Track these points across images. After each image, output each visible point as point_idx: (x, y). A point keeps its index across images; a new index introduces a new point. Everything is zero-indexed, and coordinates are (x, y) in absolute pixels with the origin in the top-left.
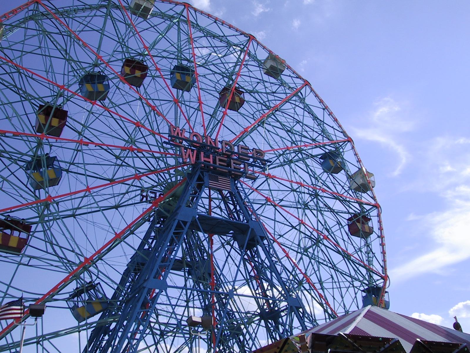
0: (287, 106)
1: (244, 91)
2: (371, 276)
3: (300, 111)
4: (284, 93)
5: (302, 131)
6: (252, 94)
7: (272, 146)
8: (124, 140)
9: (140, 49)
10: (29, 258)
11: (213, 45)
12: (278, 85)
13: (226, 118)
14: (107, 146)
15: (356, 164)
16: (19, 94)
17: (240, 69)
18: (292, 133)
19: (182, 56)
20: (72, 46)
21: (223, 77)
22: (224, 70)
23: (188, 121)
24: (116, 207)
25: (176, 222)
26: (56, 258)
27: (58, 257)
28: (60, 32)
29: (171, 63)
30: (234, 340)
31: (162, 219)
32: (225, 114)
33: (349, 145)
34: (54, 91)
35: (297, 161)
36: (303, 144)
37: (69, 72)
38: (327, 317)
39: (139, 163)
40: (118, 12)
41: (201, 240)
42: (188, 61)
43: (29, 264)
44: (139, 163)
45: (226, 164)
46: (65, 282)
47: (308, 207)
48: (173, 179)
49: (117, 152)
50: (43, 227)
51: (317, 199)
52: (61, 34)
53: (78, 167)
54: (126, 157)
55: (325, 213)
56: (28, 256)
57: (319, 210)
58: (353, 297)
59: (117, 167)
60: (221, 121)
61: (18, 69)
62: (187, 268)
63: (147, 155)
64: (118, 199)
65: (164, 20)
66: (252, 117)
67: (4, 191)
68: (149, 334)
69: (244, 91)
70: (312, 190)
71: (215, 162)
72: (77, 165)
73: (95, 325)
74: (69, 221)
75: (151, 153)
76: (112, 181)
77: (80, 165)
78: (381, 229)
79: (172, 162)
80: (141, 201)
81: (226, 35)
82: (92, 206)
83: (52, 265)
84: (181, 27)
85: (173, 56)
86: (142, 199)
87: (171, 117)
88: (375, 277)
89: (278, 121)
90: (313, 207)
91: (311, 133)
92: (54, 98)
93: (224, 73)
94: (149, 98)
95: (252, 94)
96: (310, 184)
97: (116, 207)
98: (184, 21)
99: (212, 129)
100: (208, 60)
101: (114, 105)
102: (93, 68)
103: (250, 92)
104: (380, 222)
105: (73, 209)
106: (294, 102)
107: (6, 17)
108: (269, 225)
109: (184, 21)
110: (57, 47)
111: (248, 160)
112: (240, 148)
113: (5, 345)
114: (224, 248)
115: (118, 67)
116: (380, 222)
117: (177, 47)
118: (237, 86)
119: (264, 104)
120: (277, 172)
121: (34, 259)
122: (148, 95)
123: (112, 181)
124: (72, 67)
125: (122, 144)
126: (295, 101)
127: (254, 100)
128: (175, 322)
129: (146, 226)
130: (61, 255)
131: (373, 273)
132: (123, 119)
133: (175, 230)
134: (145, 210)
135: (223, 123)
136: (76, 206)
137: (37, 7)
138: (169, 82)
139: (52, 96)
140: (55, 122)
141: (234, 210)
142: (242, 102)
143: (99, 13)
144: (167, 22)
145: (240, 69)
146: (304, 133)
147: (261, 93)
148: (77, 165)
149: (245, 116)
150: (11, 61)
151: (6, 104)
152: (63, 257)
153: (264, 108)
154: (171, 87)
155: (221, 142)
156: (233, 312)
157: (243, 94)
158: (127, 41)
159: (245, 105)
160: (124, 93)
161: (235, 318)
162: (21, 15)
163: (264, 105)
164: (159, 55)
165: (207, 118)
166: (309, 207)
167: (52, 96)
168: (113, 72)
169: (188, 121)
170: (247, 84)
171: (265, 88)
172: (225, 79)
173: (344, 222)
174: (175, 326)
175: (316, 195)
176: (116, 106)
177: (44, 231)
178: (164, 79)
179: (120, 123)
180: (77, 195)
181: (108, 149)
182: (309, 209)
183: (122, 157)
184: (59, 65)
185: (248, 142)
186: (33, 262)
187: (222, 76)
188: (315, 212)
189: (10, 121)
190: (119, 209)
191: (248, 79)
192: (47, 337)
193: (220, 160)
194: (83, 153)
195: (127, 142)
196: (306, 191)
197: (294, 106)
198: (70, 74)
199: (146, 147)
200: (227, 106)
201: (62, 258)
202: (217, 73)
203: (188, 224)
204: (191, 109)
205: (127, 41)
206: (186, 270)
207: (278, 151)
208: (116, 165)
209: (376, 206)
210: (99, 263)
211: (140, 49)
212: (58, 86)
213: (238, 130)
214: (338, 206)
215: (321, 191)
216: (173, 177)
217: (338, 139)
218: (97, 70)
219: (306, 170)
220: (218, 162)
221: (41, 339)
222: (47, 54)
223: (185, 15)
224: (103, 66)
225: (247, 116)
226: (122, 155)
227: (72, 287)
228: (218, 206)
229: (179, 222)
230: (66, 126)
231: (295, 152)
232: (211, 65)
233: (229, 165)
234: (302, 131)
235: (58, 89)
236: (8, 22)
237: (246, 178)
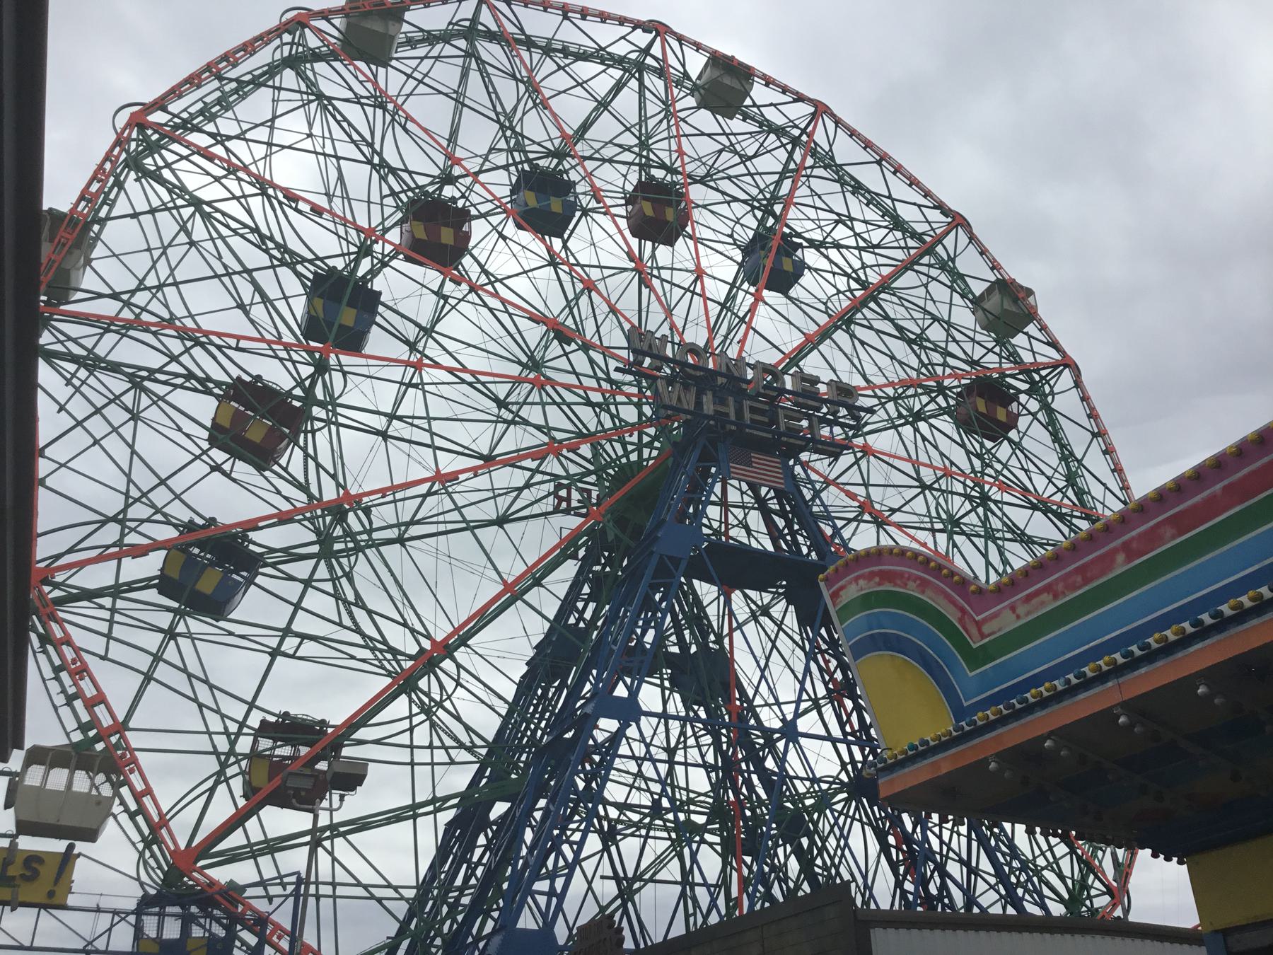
0: (909, 279)
1: (805, 244)
3: (940, 292)
4: (900, 248)
5: (947, 342)
6: (822, 250)
7: (871, 378)
8: (519, 362)
9: (551, 140)
10: (299, 640)
11: (728, 131)
12: (886, 227)
13: (762, 309)
14: (473, 373)
15: (1086, 423)
16: (267, 251)
17: (794, 188)
18: (921, 347)
19: (652, 156)
20: (389, 133)
21: (753, 208)
22: (755, 192)
23: (669, 312)
24: (501, 521)
25: (654, 561)
26: (357, 639)
27: (363, 635)
28: (356, 98)
29: (625, 176)
30: (788, 846)
31: (606, 554)
32: (758, 298)
33: (1066, 378)
34: (348, 242)
35: (935, 416)
36: (948, 371)
37: (382, 198)
39: (556, 418)
40: (495, 48)
41: (701, 603)
42: (671, 170)
43: (297, 655)
44: (556, 418)
45: (766, 420)
47: (961, 529)
48: (634, 457)
49: (501, 391)
50: (331, 568)
52: (359, 103)
53: (412, 425)
54: (525, 403)
55: (1008, 545)
56: (297, 635)
57: (990, 535)
59: (501, 427)
60: (747, 320)
61: (263, 186)
62: (669, 671)
63: (569, 397)
64: (503, 502)
65: (604, 67)
66: (824, 309)
67: (234, 480)
68: (652, 793)
69: (805, 244)
70: (971, 484)
71: (739, 412)
72: (410, 420)
73: (456, 801)
74: (392, 552)
75: (581, 392)
76: (489, 460)
77: (416, 422)
79: (629, 414)
80: (556, 510)
81: (758, 103)
82: (448, 517)
83: (353, 657)
84: (647, 82)
85: (628, 157)
86: (559, 504)
87: (628, 305)
89: (886, 317)
90: (977, 529)
91: (968, 347)
92: (350, 262)
93: (754, 199)
94: (575, 262)
95: (822, 250)
96: (968, 471)
97: (501, 521)
98: (654, 70)
99: (726, 337)
100: (715, 166)
101: (493, 279)
102: (441, 189)
103: (812, 244)
105: (398, 525)
106: (924, 269)
107: (228, 61)
109: (654, 70)
110: (350, 136)
111: (818, 410)
113: (244, 847)
114: (757, 621)
115: (500, 183)
117: (637, 134)
118: (786, 230)
119: (854, 275)
120: (883, 441)
121: (312, 643)
122: (572, 254)
123: (489, 460)
124: (390, 188)
125: (515, 370)
126: (930, 266)
127: (719, 197)
128: (646, 800)
129: (569, 569)
130: (370, 631)
132: (511, 310)
133: (652, 579)
134: (565, 533)
135: (753, 325)
136: (407, 518)
137: (302, 36)
138: (623, 223)
139: (343, 255)
140: (348, 316)
141: (786, 531)
142: (801, 267)
143: (449, 50)
144: (611, 71)
145: (794, 188)
146: (953, 348)
147: (847, 247)
148: (410, 420)
149: (804, 307)
150: (245, 168)
151: (235, 273)
152: (377, 636)
153: (854, 285)
154: (627, 233)
155: (753, 367)
157: (800, 250)
158: (521, 119)
159: (807, 279)
160: (515, 248)
161: (788, 793)
162: (264, 56)
163: (853, 279)
164: (597, 156)
165: (714, 309)
166: (964, 528)
167: (343, 255)
168: (490, 198)
169: (669, 312)
170: (810, 225)
172: (756, 211)
174: (647, 811)
176: (497, 280)
177: (334, 580)
178: (613, 216)
179: (504, 318)
180: (410, 492)
181: (476, 381)
182: (963, 533)
183: (513, 404)
184: (358, 176)
185: (812, 364)
186: (309, 648)
187: (751, 206)
188: (980, 542)
189: (247, 313)
190: (505, 526)
191: (811, 213)
192: (342, 829)
193: (752, 410)
194: (424, 392)
195: (524, 366)
196: (959, 488)
197: (924, 279)
198: (386, 201)
199: (572, 380)
200: (763, 280)
201: (372, 639)
204: (675, 289)
205: (521, 119)
206: (667, 674)
207: (884, 389)
208: (499, 420)
210: (461, 654)
211: (551, 140)
212: (359, 230)
213: (791, 340)
215: (995, 489)
216: (633, 451)
217: (1040, 359)
218: (448, 191)
219: (957, 438)
220: (747, 415)
221: (328, 834)
222: (329, 150)
223: (658, 54)
224: (469, 180)
225: (807, 304)
226: (512, 399)
228: (740, 522)
230: (374, 327)
231: (928, 390)
232: (723, 178)
233: (774, 420)
234: (947, 342)
235: (359, 236)
236: (233, 74)
237: (815, 453)
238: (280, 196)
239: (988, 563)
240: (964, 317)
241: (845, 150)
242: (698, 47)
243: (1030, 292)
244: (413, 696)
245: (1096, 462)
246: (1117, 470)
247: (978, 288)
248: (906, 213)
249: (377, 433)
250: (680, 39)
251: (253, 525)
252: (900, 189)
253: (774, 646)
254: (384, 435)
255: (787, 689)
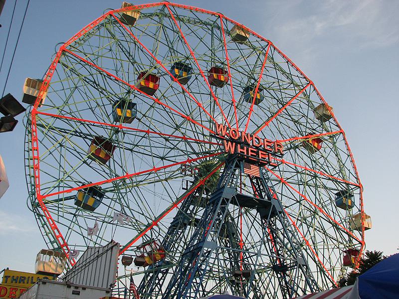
0: (295, 101)
2: (350, 241)
15: (346, 152)
25: (222, 198)
38: (319, 270)
46: (137, 237)
51: (316, 179)
58: (338, 257)
67: (90, 167)
78: (361, 205)
84: (214, 32)
88: (354, 242)
104: (361, 199)
108: (285, 202)
112: (265, 141)
116: (361, 199)
131: (353, 238)
156: (250, 264)
171: (280, 86)
173: (333, 197)
175: (315, 177)
193: (252, 151)
202: (275, 98)
203: (230, 201)
209: (359, 187)
214: (330, 184)
220: (250, 153)
227: (139, 242)
229: (223, 199)
238: (106, 75)
239: (316, 198)
240: (311, 115)
241: (278, 59)
242: (232, 22)
243: (332, 108)
244: (144, 237)
245: (349, 165)
246: (355, 167)
247: (316, 105)
248: (296, 80)
249: (130, 150)
250: (226, 19)
251: (100, 183)
252: (294, 72)
253: (253, 225)
254: (131, 150)
255: (257, 239)
